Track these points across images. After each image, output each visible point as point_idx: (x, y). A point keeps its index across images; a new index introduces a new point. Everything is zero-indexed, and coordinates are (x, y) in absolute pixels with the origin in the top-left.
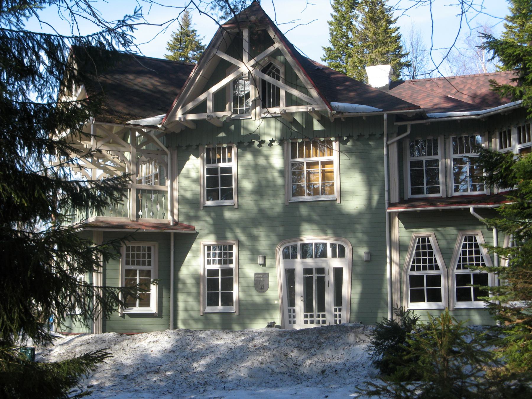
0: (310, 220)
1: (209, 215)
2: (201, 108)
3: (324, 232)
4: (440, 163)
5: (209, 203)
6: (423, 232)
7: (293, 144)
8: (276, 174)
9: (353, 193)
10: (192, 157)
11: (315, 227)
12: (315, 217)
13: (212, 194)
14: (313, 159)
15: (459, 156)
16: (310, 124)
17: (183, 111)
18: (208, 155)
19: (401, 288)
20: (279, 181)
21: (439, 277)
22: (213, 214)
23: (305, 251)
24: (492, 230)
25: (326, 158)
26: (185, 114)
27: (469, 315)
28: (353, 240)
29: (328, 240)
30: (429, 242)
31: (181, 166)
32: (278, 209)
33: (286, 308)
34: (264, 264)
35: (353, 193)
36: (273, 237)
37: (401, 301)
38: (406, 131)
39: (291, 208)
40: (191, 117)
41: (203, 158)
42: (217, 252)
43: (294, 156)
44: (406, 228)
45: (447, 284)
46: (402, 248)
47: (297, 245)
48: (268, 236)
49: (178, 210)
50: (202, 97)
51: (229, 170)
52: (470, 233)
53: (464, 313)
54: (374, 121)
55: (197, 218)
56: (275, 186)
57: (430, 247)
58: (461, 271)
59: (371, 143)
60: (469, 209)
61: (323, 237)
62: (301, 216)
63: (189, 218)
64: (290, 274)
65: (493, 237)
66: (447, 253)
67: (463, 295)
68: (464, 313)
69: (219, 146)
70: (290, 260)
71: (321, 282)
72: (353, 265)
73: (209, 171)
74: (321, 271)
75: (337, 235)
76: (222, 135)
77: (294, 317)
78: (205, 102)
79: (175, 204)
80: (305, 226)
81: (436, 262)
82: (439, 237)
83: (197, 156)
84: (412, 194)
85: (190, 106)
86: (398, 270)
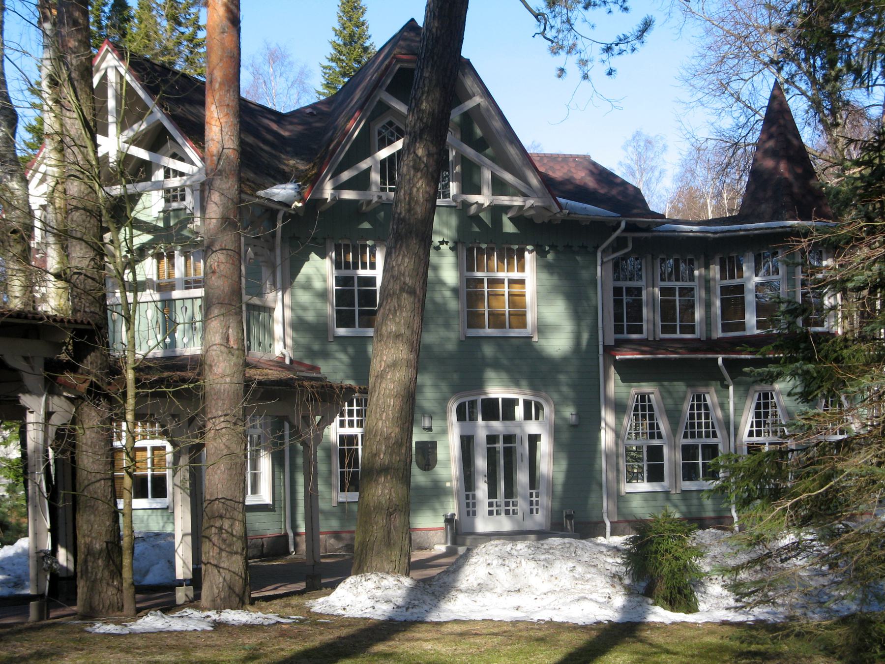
0: (496, 366)
1: (345, 351)
2: (361, 182)
3: (516, 383)
4: (644, 293)
5: (342, 331)
6: (647, 388)
7: (470, 251)
8: (448, 294)
9: (555, 328)
10: (313, 256)
11: (504, 375)
12: (505, 362)
13: (344, 319)
14: (501, 275)
15: (667, 284)
16: (497, 223)
17: (334, 183)
18: (338, 254)
19: (617, 464)
20: (453, 305)
21: (660, 448)
22: (351, 350)
23: (491, 409)
24: (727, 387)
25: (515, 275)
26: (338, 187)
27: (700, 499)
28: (556, 396)
29: (520, 396)
30: (649, 401)
31: (295, 269)
32: (451, 347)
33: (463, 493)
34: (430, 429)
35: (555, 328)
36: (444, 387)
37: (618, 482)
38: (626, 246)
39: (470, 345)
40: (348, 195)
41: (331, 258)
42: (355, 408)
43: (470, 269)
44: (623, 380)
45: (671, 457)
46: (619, 408)
47: (476, 401)
48: (436, 386)
49: (293, 339)
50: (364, 165)
51: (371, 281)
52: (702, 390)
53: (694, 495)
54: (601, 229)
55: (325, 355)
56: (447, 311)
57: (651, 408)
58: (689, 441)
59: (578, 258)
60: (717, 359)
61: (516, 390)
62: (483, 358)
63: (312, 353)
64: (467, 443)
65: (728, 397)
66: (673, 416)
67: (690, 473)
68: (694, 495)
69: (363, 243)
70: (467, 423)
71: (509, 453)
72: (556, 433)
73: (339, 281)
74: (509, 438)
75: (535, 388)
76: (366, 225)
77: (474, 505)
78: (368, 171)
79: (289, 331)
80: (490, 374)
81: (658, 428)
82: (665, 394)
83: (323, 256)
84: (723, 331)
85: (346, 176)
86: (614, 440)
